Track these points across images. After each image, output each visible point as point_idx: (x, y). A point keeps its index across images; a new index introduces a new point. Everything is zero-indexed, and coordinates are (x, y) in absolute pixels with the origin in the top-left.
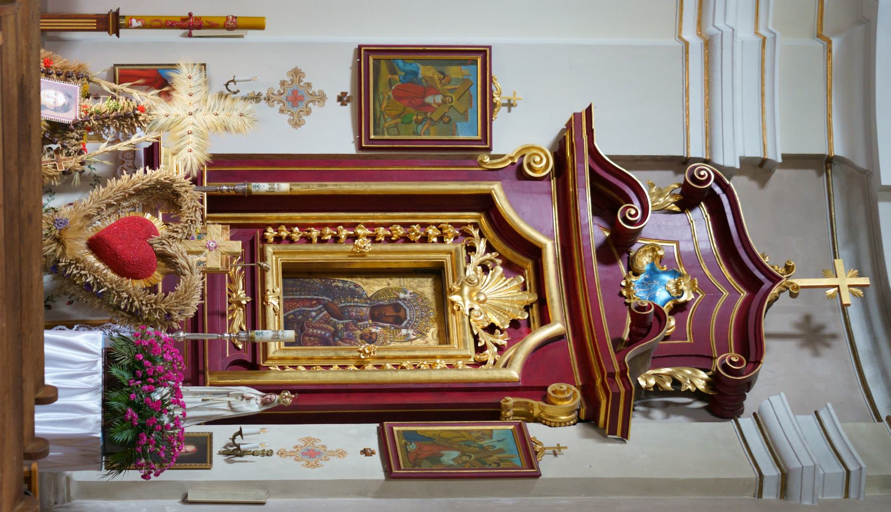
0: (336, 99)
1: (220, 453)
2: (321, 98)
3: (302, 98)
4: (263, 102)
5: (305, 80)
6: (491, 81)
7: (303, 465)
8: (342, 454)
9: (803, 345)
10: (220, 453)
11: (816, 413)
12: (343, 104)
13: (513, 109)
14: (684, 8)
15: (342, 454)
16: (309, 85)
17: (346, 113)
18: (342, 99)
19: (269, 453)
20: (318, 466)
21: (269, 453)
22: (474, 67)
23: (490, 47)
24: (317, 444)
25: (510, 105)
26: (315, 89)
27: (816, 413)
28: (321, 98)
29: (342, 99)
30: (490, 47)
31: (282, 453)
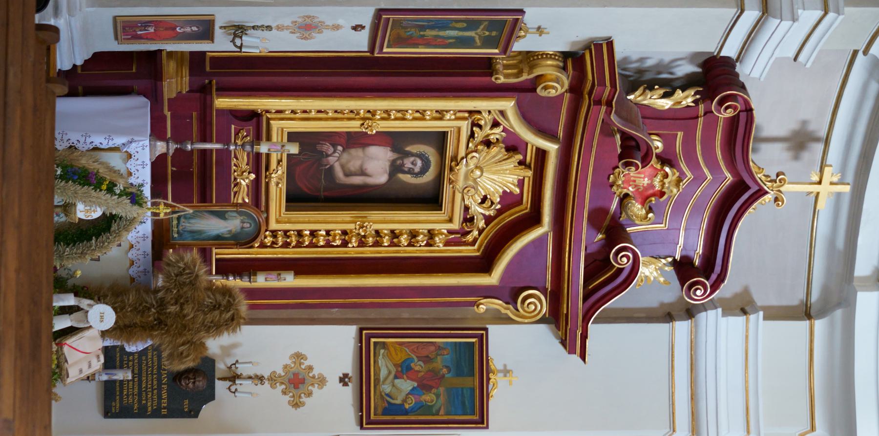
0: (338, 380)
1: (221, 27)
2: (322, 381)
3: (303, 381)
4: (267, 384)
5: (307, 363)
6: (488, 360)
7: (297, 37)
8: (337, 27)
9: (789, 149)
10: (221, 27)
11: (795, 59)
12: (346, 384)
13: (508, 368)
14: (657, 121)
15: (337, 27)
16: (310, 368)
17: (348, 394)
18: (344, 380)
19: (269, 28)
20: (312, 38)
21: (269, 28)
22: (470, 379)
23: (487, 427)
24: (316, 20)
25: (506, 372)
26: (316, 372)
27: (795, 59)
28: (322, 381)
29: (344, 380)
30: (487, 427)
31: (279, 28)
